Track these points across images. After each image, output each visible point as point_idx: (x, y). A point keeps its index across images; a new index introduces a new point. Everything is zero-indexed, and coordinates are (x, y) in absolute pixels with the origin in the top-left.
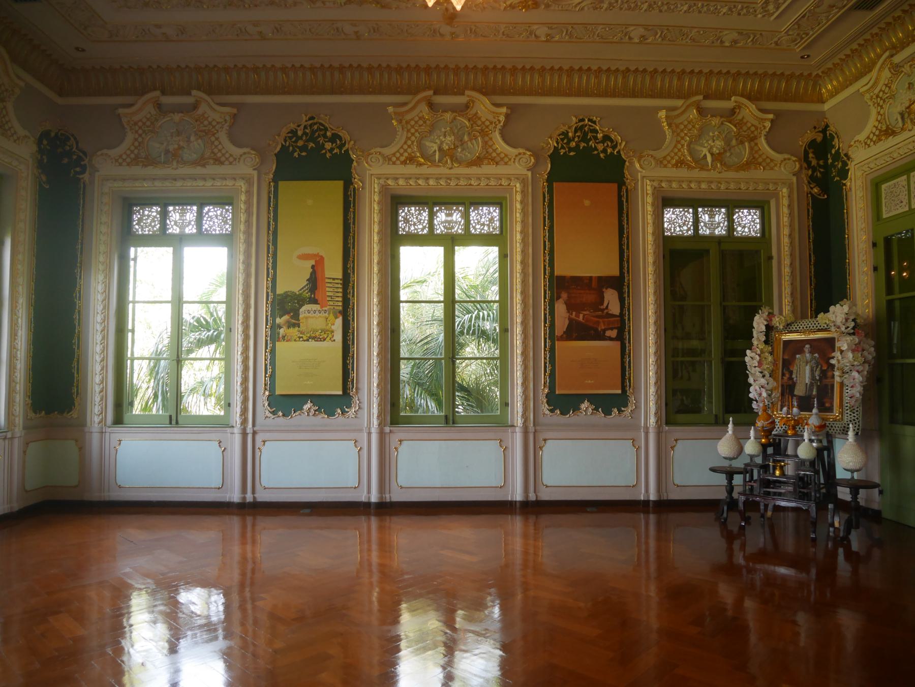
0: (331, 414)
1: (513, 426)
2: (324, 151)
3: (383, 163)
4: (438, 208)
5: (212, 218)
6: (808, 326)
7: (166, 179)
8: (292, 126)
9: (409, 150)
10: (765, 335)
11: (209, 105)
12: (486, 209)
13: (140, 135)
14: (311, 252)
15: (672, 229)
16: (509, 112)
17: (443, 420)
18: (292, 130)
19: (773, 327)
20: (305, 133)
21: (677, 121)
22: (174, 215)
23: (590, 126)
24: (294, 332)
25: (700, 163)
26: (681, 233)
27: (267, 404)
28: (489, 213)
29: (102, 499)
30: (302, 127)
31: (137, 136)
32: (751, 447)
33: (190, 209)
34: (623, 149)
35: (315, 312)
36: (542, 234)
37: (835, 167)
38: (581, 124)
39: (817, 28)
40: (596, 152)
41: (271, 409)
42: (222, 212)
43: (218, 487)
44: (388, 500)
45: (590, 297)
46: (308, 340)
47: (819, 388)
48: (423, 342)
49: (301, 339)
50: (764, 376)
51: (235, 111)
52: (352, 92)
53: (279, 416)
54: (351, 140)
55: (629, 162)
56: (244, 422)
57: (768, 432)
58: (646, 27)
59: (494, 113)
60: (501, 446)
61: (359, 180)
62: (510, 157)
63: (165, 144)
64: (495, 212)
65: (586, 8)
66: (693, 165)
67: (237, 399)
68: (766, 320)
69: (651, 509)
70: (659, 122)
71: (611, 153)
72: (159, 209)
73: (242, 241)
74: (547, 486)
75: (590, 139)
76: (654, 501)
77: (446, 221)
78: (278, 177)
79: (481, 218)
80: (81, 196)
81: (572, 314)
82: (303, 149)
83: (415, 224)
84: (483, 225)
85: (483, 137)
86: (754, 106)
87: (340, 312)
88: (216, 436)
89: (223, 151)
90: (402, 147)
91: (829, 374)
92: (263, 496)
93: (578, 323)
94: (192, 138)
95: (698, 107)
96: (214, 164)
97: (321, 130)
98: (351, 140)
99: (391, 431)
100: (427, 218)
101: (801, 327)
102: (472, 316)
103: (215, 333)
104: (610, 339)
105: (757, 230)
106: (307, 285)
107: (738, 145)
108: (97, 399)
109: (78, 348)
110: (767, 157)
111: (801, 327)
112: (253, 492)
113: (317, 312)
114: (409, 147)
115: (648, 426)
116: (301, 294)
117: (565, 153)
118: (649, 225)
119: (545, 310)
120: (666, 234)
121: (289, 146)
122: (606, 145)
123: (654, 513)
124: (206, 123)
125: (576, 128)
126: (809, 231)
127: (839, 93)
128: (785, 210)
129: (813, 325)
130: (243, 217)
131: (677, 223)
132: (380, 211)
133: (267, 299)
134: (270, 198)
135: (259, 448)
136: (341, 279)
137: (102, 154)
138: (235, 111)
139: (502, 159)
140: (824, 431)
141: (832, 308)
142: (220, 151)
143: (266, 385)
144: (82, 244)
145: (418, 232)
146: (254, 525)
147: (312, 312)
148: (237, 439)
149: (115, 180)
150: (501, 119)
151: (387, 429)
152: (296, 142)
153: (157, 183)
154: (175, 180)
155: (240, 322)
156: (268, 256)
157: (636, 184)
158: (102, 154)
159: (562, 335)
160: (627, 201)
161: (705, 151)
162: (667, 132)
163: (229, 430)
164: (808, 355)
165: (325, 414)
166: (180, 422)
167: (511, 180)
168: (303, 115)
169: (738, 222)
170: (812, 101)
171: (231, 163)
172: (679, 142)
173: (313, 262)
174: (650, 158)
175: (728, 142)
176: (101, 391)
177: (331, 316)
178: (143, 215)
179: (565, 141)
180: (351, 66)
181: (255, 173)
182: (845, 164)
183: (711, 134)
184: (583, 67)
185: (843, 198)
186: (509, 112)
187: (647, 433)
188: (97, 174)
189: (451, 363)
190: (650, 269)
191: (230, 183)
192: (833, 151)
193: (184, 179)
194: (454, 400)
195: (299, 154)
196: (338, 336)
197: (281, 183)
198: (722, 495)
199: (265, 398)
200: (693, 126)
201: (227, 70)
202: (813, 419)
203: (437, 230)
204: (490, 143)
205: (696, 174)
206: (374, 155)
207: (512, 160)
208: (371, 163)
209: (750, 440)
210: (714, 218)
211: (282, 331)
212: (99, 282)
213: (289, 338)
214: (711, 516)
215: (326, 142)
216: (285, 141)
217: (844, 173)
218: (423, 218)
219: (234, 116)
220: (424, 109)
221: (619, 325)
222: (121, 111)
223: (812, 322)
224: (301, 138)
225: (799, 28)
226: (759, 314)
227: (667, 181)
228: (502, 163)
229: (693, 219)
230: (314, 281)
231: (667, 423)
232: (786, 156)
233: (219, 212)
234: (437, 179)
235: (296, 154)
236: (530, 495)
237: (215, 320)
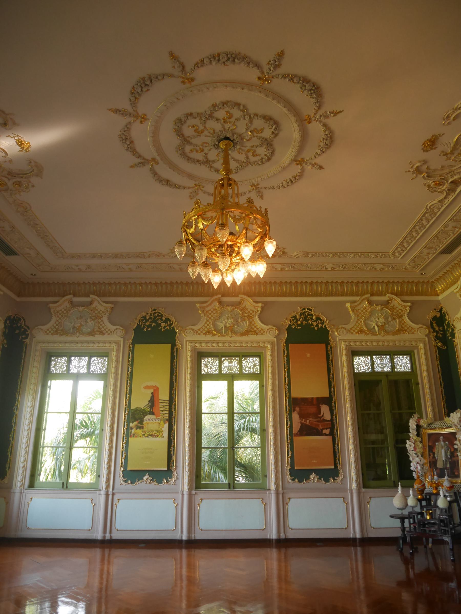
0: (160, 482)
1: (269, 490)
2: (161, 328)
3: (193, 334)
4: (224, 359)
7: (73, 343)
8: (144, 314)
9: (208, 327)
10: (416, 431)
11: (99, 302)
13: (60, 318)
14: (151, 385)
15: (359, 368)
16: (263, 305)
17: (227, 486)
18: (143, 316)
19: (421, 426)
20: (150, 318)
21: (357, 308)
22: (75, 361)
23: (308, 312)
24: (140, 431)
25: (372, 331)
26: (364, 370)
27: (121, 476)
28: (253, 361)
29: (17, 537)
30: (149, 314)
31: (58, 319)
32: (411, 501)
33: (84, 359)
34: (328, 325)
35: (152, 420)
36: (284, 373)
37: (449, 331)
38: (303, 311)
39: (424, 262)
40: (312, 327)
41: (124, 479)
42: (102, 361)
44: (193, 538)
45: (312, 410)
46: (148, 437)
47: (450, 463)
48: (216, 437)
49: (144, 436)
50: (418, 456)
51: (112, 306)
52: (177, 295)
53: (129, 484)
54: (176, 322)
55: (331, 332)
56: (108, 487)
57: (421, 491)
58: (333, 264)
59: (255, 306)
60: (263, 503)
61: (180, 344)
62: (264, 330)
63: (73, 323)
64: (256, 360)
65: (300, 257)
66: (368, 332)
67: (104, 473)
68: (417, 422)
69: (358, 544)
70: (347, 309)
71: (321, 327)
72: (66, 359)
73: (113, 378)
74: (292, 529)
75: (309, 320)
76: (359, 539)
77: (229, 366)
78: (136, 341)
79: (249, 364)
80: (24, 351)
81: (302, 420)
82: (149, 326)
83: (211, 368)
84: (250, 368)
85: (249, 320)
86: (399, 299)
87: (167, 420)
88: (90, 496)
89: (105, 327)
90: (204, 325)
91: (455, 454)
92: (116, 536)
93: (306, 425)
94: (89, 320)
95: (368, 300)
96: (99, 334)
97: (159, 316)
98: (176, 322)
99: (196, 493)
100: (218, 365)
101: (437, 426)
102: (245, 420)
103: (92, 430)
104: (326, 435)
106: (149, 404)
107: (392, 320)
108: (21, 471)
109: (13, 440)
110: (410, 327)
111: (437, 426)
112: (110, 532)
113: (154, 420)
114: (208, 325)
115: (352, 489)
116: (145, 409)
117: (295, 328)
118: (345, 367)
119: (286, 418)
120: (355, 371)
121: (141, 325)
122: (318, 322)
123: (360, 546)
124: (96, 312)
125: (300, 314)
126: (438, 368)
127: (445, 291)
128: (423, 357)
130: (114, 365)
132: (192, 361)
133: (125, 412)
134: (129, 353)
135: (115, 504)
136: (168, 401)
137: (38, 329)
138: (112, 306)
139: (260, 331)
140: (453, 490)
141: (451, 414)
142: (103, 327)
143: (122, 464)
144: (22, 378)
145: (213, 372)
146: (109, 555)
147: (151, 420)
148: (103, 497)
149: (44, 343)
150: (259, 310)
151: (193, 492)
152: (145, 322)
153: (67, 345)
154: (77, 343)
155: (109, 425)
156: (127, 387)
157: (336, 344)
158: (38, 329)
159: (297, 433)
160: (331, 354)
161: (374, 324)
162: (352, 315)
163: (98, 492)
164: (442, 443)
165: (156, 482)
166: (68, 487)
167: (265, 343)
168: (150, 308)
169: (397, 363)
170: (432, 295)
171: (109, 334)
172: (359, 320)
173: (152, 391)
174: (343, 329)
175: (386, 318)
176: (23, 467)
177: (162, 422)
178: (57, 362)
179: (295, 321)
180: (177, 282)
181: (122, 340)
182: (453, 330)
183: (377, 315)
185: (454, 348)
186: (263, 305)
187: (352, 494)
188: (34, 339)
189: (232, 450)
190: (347, 393)
191: (107, 345)
192: (446, 322)
193: (82, 343)
194: (234, 473)
195: (146, 329)
196: (166, 434)
197: (136, 346)
198: (398, 534)
199: (121, 472)
200: (366, 311)
201: (110, 284)
202: (446, 482)
203: (224, 371)
204: (253, 323)
205: (370, 337)
206: (188, 330)
207: (266, 332)
208: (187, 334)
209: (410, 497)
210: (383, 361)
211: (133, 431)
212: (29, 401)
213: (137, 435)
214: (394, 548)
215: (162, 322)
216: (139, 322)
218: (216, 364)
219: (112, 309)
220: (216, 304)
221: (331, 426)
222: (51, 305)
224: (148, 320)
225: (414, 262)
226: (412, 418)
227: (354, 342)
228: (260, 333)
229: (371, 362)
230: (153, 402)
231: (364, 487)
232: (421, 326)
233: (100, 361)
234: (223, 343)
235: (145, 330)
236: (281, 535)
237: (91, 423)
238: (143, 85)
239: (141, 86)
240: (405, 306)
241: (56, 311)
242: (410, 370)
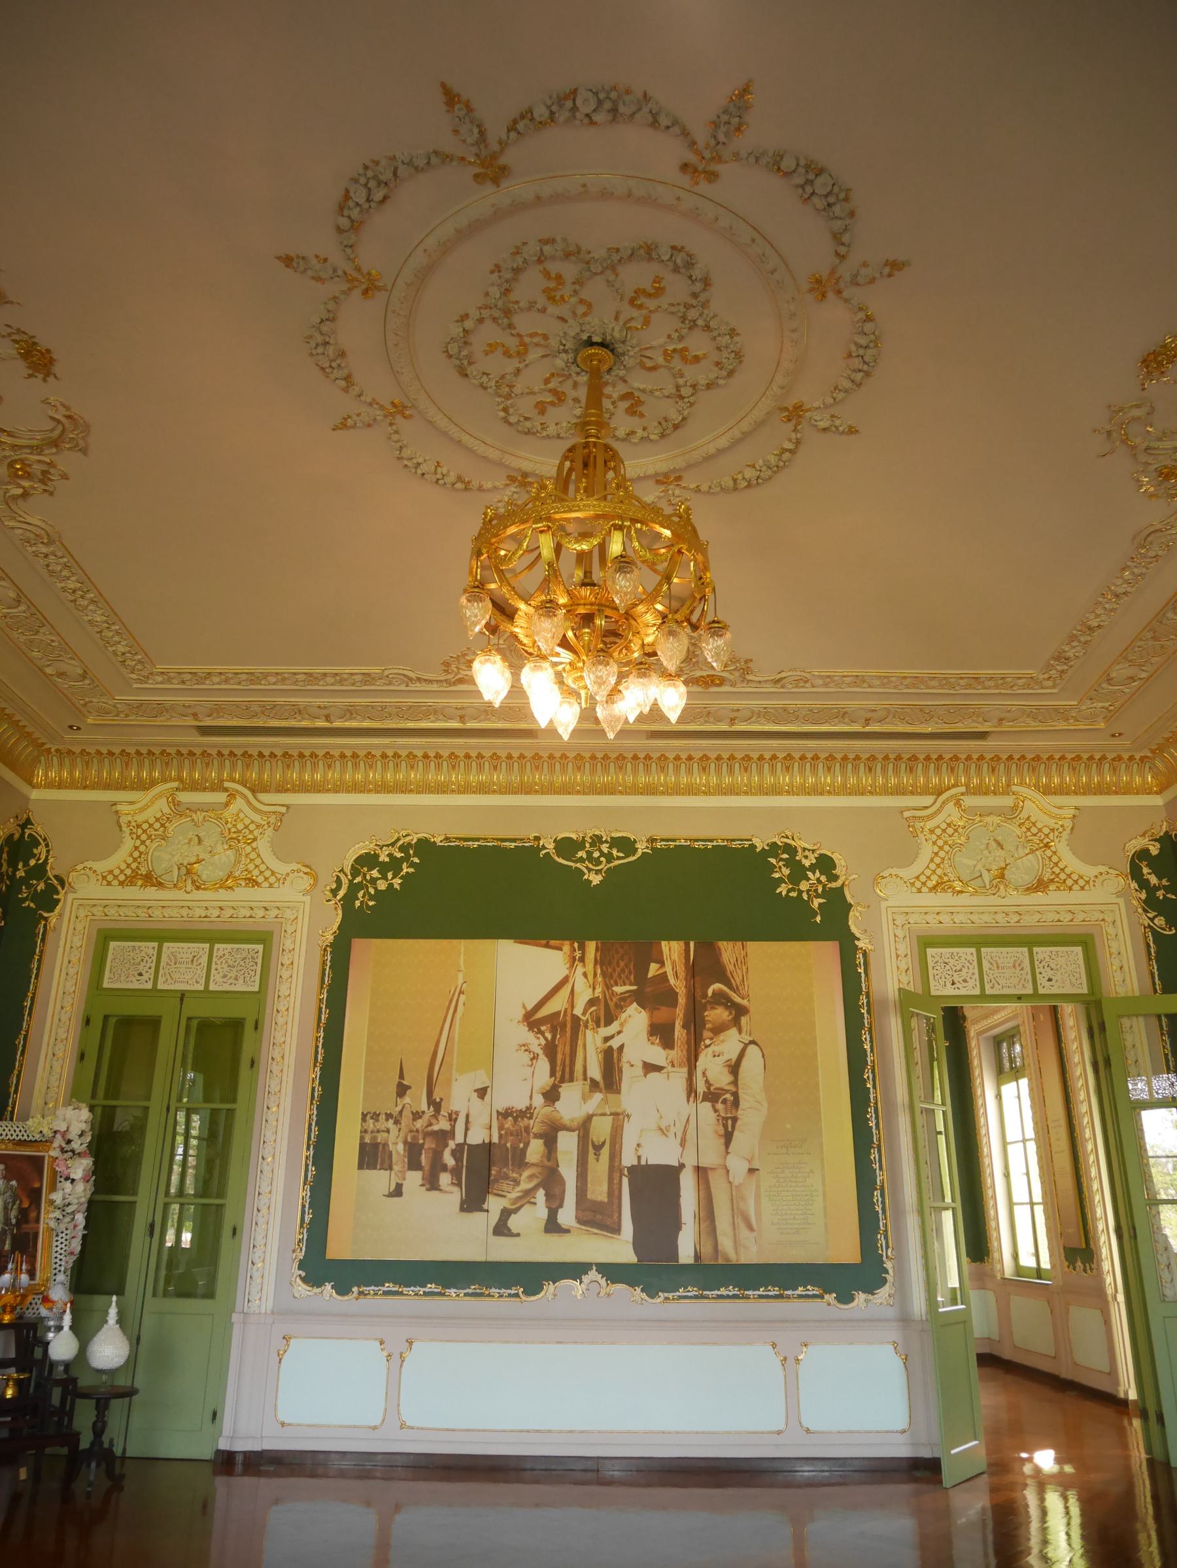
6: (9, 1133)
13: (143, 842)
31: (138, 843)
129: (18, 1132)
217: (48, 901)
223: (10, 1127)
238: (372, 184)
239: (366, 185)
241: (134, 824)
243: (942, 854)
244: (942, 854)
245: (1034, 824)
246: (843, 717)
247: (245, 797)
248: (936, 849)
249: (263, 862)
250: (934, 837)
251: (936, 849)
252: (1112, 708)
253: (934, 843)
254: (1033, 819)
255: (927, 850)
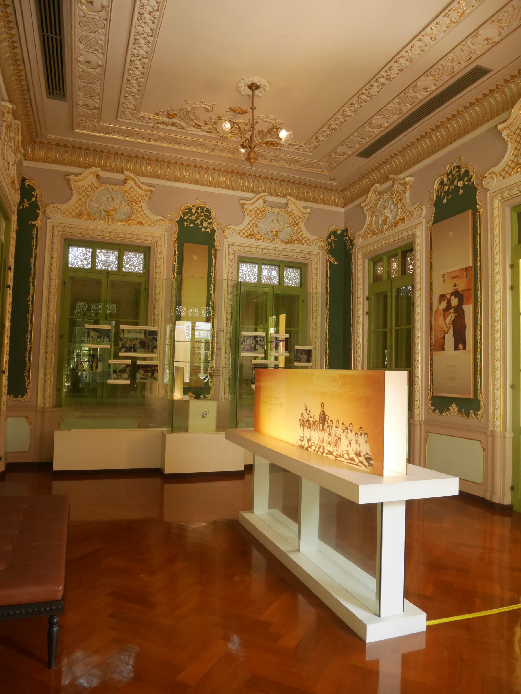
5: (252, 274)
12: (134, 255)
26: (82, 266)
43: (24, 450)
64: (140, 257)
96: (298, 243)
105: (140, 268)
131: (79, 258)
169: (127, 261)
184: (159, 159)
240: (304, 213)
242: (141, 272)
243: (253, 222)
244: (253, 222)
245: (293, 214)
246: (202, 146)
247: (134, 180)
248: (251, 219)
249: (147, 216)
250: (251, 214)
251: (251, 219)
252: (331, 166)
253: (251, 216)
254: (293, 212)
255: (247, 219)
